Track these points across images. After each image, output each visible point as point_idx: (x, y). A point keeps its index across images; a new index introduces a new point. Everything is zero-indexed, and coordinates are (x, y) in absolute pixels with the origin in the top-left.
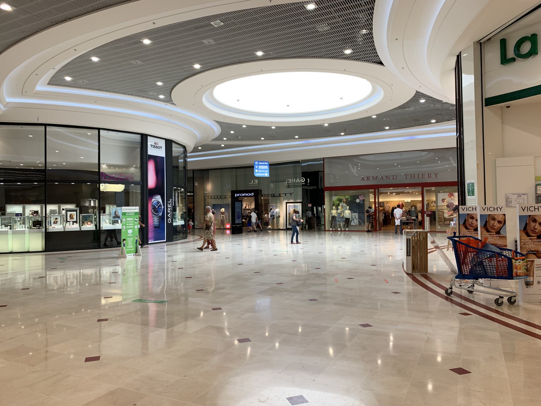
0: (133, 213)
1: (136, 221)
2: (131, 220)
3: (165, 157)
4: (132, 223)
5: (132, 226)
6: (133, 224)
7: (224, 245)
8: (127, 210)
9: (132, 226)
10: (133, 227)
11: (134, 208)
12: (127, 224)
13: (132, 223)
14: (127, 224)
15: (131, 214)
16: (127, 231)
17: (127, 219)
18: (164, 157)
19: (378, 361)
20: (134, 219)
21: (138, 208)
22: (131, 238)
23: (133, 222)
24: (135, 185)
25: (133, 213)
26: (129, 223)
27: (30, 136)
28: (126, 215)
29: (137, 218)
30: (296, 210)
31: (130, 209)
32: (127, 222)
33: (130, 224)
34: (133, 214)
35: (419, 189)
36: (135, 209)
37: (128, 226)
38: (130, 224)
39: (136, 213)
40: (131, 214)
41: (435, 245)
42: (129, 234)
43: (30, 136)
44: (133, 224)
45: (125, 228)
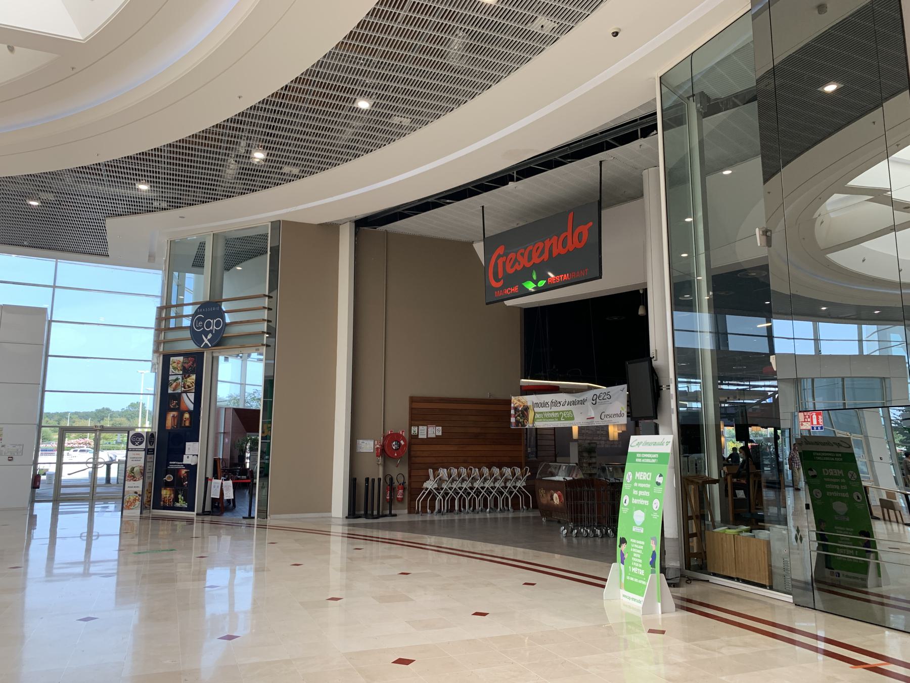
0: (654, 456)
1: (658, 484)
2: (644, 478)
3: (261, 408)
4: (647, 489)
5: (644, 498)
6: (647, 494)
7: (245, 575)
8: (641, 446)
9: (644, 498)
10: (646, 503)
11: (657, 441)
12: (635, 492)
13: (647, 489)
14: (635, 492)
15: (648, 460)
16: (632, 515)
17: (637, 475)
18: (259, 411)
19: (835, 83)
20: (653, 477)
21: (671, 441)
22: (640, 542)
23: (649, 486)
24: (500, 395)
25: (654, 456)
26: (639, 489)
27: (759, 326)
28: (635, 462)
29: (661, 475)
30: (347, 515)
31: (647, 444)
32: (636, 484)
33: (641, 493)
34: (654, 461)
35: (90, 438)
36: (662, 444)
37: (637, 497)
38: (641, 493)
39: (662, 457)
40: (648, 460)
41: (665, 444)
42: (636, 525)
43: (759, 326)
44: (647, 494)
45: (627, 502)
